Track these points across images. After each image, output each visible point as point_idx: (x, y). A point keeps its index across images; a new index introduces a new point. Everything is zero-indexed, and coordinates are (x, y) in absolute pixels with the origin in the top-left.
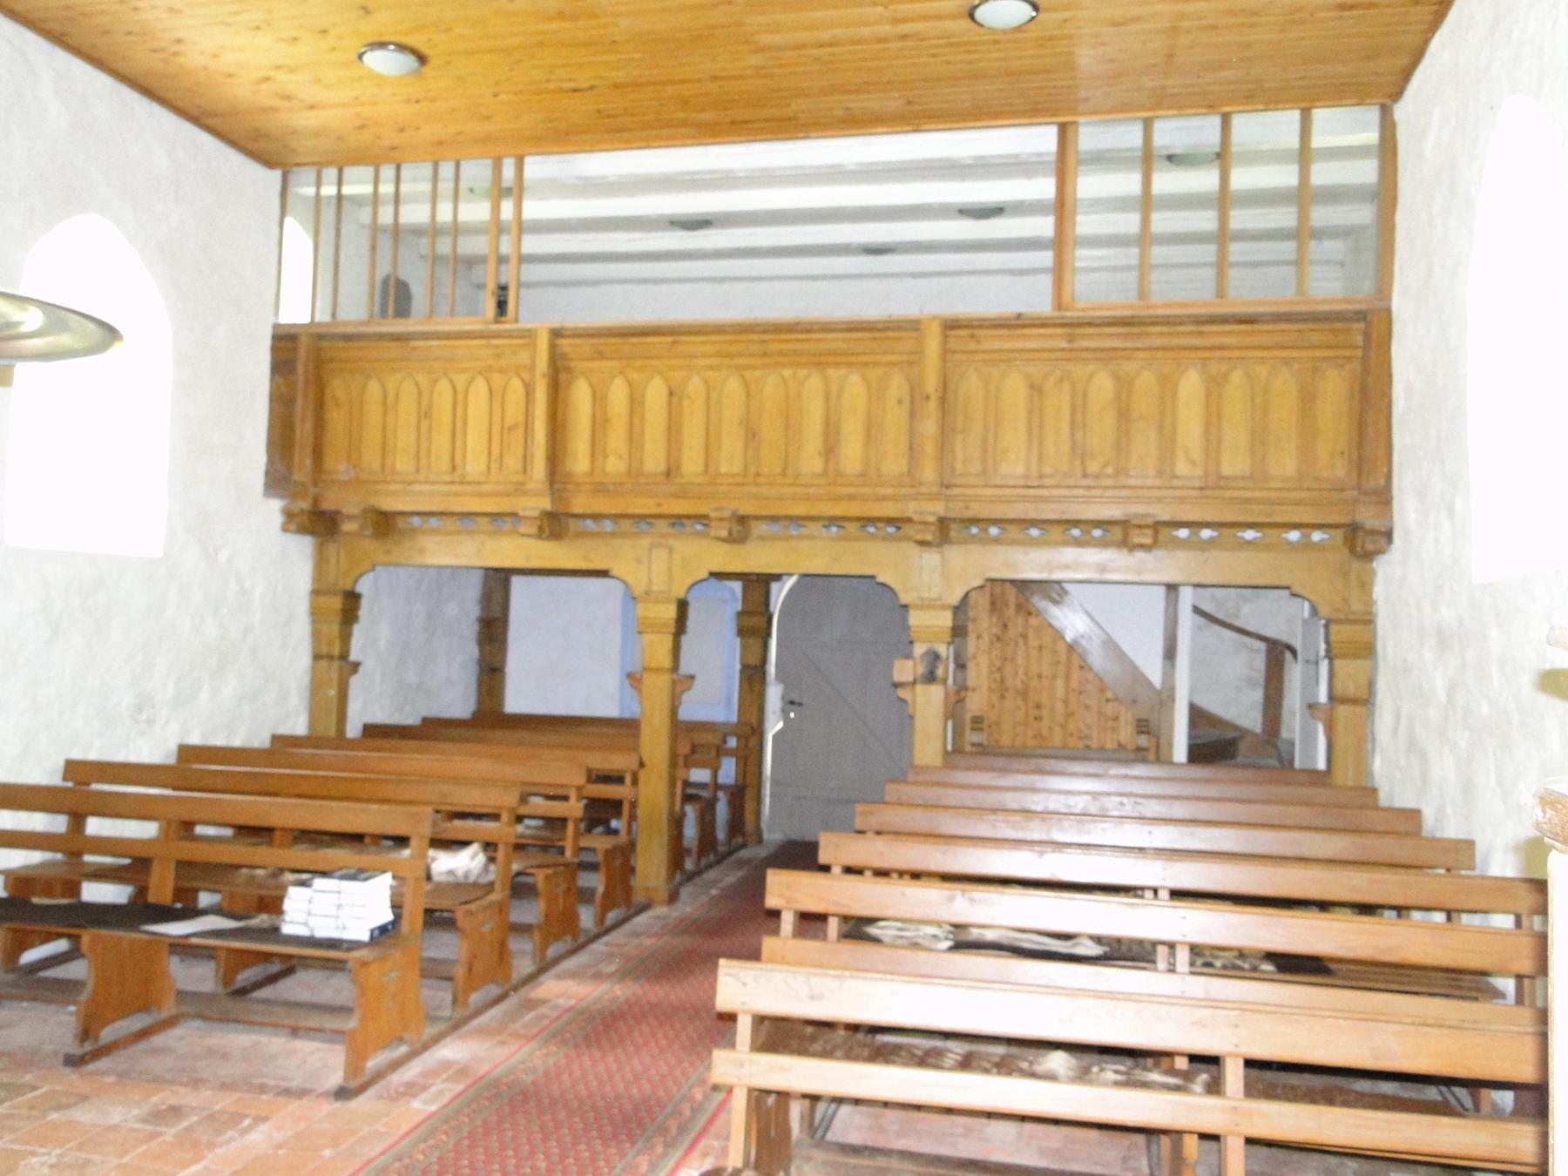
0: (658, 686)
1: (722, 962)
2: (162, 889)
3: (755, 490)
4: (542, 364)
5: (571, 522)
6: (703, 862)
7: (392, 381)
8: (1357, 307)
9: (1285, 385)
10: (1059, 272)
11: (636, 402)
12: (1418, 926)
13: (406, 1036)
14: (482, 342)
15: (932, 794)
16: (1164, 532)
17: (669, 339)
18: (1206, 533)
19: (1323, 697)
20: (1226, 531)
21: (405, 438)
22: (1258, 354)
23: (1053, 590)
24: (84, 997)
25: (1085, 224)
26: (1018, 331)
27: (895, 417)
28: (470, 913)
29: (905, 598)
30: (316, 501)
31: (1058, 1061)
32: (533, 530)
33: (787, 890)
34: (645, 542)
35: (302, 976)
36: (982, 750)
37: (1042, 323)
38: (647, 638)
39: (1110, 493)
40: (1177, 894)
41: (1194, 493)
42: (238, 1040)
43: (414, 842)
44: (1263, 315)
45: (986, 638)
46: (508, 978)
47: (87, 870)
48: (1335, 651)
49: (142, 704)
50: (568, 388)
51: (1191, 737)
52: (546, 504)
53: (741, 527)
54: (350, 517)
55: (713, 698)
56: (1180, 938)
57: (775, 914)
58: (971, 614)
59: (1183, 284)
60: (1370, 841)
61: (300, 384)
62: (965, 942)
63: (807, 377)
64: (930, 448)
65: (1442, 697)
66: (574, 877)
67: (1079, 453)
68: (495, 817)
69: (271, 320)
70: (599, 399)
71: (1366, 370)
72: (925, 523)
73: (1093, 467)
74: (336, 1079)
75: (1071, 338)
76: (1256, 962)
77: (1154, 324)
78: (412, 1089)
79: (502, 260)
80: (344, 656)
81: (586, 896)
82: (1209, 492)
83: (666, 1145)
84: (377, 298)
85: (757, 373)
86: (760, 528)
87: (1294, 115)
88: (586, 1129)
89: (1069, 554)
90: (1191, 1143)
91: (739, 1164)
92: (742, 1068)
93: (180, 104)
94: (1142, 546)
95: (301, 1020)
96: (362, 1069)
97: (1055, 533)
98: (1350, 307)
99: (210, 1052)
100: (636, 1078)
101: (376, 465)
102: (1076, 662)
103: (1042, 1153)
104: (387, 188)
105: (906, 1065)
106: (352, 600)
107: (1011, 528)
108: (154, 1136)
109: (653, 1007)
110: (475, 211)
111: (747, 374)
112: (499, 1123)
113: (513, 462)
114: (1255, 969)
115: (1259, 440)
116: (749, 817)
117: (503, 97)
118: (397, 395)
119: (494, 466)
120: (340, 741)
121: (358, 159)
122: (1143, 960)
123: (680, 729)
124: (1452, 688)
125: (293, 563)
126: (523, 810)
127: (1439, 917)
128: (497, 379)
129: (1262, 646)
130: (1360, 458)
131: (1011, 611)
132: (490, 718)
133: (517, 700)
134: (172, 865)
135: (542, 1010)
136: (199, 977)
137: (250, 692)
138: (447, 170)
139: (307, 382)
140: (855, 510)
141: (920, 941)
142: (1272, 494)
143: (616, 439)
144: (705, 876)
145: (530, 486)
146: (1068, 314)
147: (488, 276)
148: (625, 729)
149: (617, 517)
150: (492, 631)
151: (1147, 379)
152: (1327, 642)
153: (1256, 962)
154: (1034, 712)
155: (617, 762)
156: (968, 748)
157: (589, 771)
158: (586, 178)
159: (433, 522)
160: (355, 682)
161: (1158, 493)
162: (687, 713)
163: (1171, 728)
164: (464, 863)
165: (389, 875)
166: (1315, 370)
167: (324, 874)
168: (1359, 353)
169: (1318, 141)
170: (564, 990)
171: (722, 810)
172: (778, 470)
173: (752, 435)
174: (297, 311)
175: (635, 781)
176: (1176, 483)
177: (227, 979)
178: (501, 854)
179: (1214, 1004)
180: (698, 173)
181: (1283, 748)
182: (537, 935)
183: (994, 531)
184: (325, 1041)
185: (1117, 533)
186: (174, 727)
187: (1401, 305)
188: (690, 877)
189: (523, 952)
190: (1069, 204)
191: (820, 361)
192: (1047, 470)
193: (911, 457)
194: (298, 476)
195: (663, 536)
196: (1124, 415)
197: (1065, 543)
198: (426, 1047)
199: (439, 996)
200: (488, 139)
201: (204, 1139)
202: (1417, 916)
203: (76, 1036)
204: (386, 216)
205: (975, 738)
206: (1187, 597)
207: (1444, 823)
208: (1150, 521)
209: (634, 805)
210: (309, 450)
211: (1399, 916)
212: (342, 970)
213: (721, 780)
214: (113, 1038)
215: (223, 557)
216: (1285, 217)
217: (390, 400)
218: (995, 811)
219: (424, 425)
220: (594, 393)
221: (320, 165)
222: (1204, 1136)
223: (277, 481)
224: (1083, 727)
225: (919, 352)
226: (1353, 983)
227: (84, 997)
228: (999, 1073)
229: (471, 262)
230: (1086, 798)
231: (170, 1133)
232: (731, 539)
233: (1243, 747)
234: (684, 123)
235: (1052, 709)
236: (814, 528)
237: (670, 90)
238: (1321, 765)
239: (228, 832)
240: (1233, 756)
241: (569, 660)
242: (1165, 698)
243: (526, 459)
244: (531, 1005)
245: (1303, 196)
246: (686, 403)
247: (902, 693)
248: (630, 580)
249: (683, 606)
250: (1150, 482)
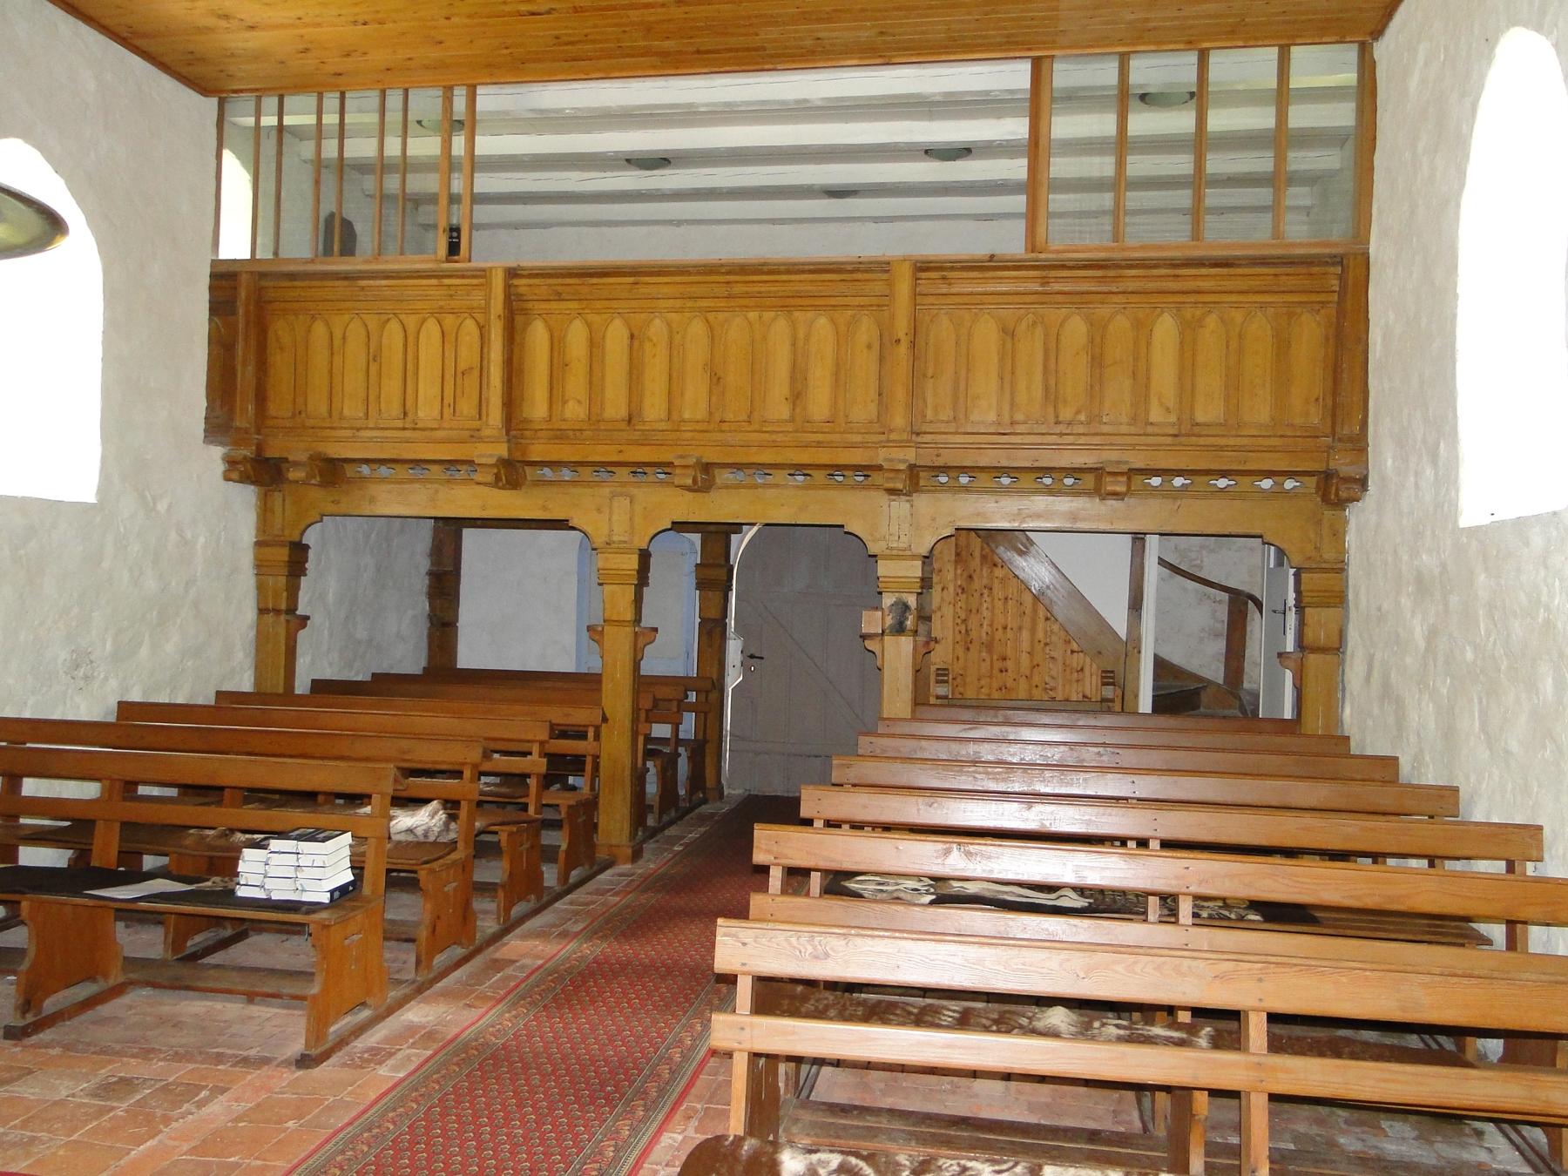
0: (619, 641)
1: (720, 921)
2: (105, 851)
3: (719, 436)
4: (497, 306)
5: (528, 470)
6: (665, 818)
7: (338, 322)
8: (1334, 251)
9: (1260, 328)
10: (1032, 216)
11: (595, 345)
12: (1395, 871)
13: (369, 1001)
14: (434, 282)
15: (906, 746)
16: (1137, 480)
17: (631, 280)
18: (1178, 482)
19: (1290, 646)
20: (1198, 479)
21: (353, 381)
22: (1234, 298)
23: (1018, 539)
24: (25, 966)
25: (1061, 167)
26: (991, 274)
27: (864, 364)
28: (432, 871)
29: (873, 549)
30: (260, 448)
31: (1058, 1017)
32: (490, 478)
33: (773, 845)
34: (606, 491)
35: (254, 939)
36: (947, 702)
37: (1017, 265)
38: (607, 588)
39: (1083, 440)
40: (1167, 845)
41: (1169, 440)
42: (193, 1007)
43: (376, 798)
44: (1238, 258)
45: (951, 589)
46: (472, 939)
47: (22, 833)
48: (1306, 600)
49: (80, 660)
50: (524, 330)
51: (1155, 689)
52: (502, 450)
53: (705, 476)
54: (296, 464)
55: (672, 654)
56: (1184, 890)
57: (764, 870)
59: (1159, 229)
60: (1356, 788)
61: (241, 326)
62: (946, 894)
63: (774, 319)
64: (900, 394)
65: (1422, 644)
66: (537, 835)
67: (1052, 396)
68: (458, 774)
69: (211, 257)
70: (557, 343)
71: (1341, 313)
72: (899, 471)
73: (1066, 413)
74: (297, 1047)
75: (1045, 281)
76: (1243, 912)
77: (1130, 267)
78: (377, 1055)
79: (454, 199)
80: (292, 610)
81: (550, 854)
82: (1183, 439)
83: (646, 1109)
84: (321, 238)
85: (721, 316)
86: (723, 476)
87: (1272, 53)
88: (562, 1095)
89: (1040, 502)
90: (1201, 1101)
91: (741, 1133)
92: (742, 1031)
93: (107, 22)
94: (1116, 495)
95: (260, 986)
96: (326, 1035)
97: (1027, 481)
98: (1327, 251)
99: (162, 1021)
100: (611, 1040)
101: (324, 409)
102: (1042, 613)
103: (1032, 1108)
104: (330, 119)
105: (902, 1024)
106: (299, 552)
107: (982, 476)
108: (102, 1111)
109: (623, 967)
110: (425, 146)
111: (711, 316)
112: (471, 1090)
113: (467, 407)
114: (1241, 919)
115: (1234, 384)
116: (709, 773)
117: (455, 20)
118: (344, 338)
119: (448, 412)
120: (288, 695)
121: (300, 87)
122: (1131, 913)
123: (642, 683)
124: (1432, 634)
125: (238, 512)
126: (486, 767)
127: (1424, 863)
128: (449, 320)
129: (1225, 596)
130: (1335, 406)
131: (976, 562)
132: (443, 673)
133: (469, 655)
134: (117, 827)
135: (509, 971)
136: (147, 943)
137: (196, 650)
138: (394, 100)
139: (247, 323)
140: (824, 457)
141: (902, 895)
142: (1245, 441)
143: (576, 384)
144: (667, 832)
145: (487, 432)
146: (1043, 256)
147: (441, 216)
148: (585, 684)
149: (576, 465)
150: (444, 585)
151: (1121, 324)
152: (1298, 591)
153: (1243, 912)
154: (998, 665)
155: (579, 716)
156: (933, 700)
157: (552, 726)
158: (542, 111)
159: (384, 471)
160: (302, 635)
161: (1129, 440)
162: (647, 669)
163: (1137, 678)
164: (421, 821)
165: (347, 838)
166: (1291, 315)
167: (282, 835)
168: (1336, 297)
169: (1296, 82)
170: (531, 949)
171: (683, 766)
172: (744, 417)
173: (716, 379)
174: (236, 244)
175: (597, 737)
176: (1150, 429)
177: (177, 944)
178: (463, 812)
179: (1239, 956)
180: (657, 106)
181: (1246, 698)
182: (501, 894)
183: (964, 480)
184: (287, 1007)
185: (1089, 481)
186: (113, 683)
187: (1378, 248)
188: (653, 833)
189: (486, 912)
190: (1043, 142)
191: (786, 304)
192: (1019, 417)
193: (880, 403)
194: (240, 422)
195: (623, 484)
196: (1097, 361)
197: (1036, 492)
198: (390, 1011)
199: (403, 959)
200: (440, 66)
201: (159, 1112)
202: (1391, 862)
203: (16, 1008)
204: (330, 149)
205: (941, 690)
206: (1152, 542)
207: (1423, 768)
208: (1125, 468)
209: (596, 758)
210: (251, 395)
211: (1375, 862)
212: (299, 933)
213: (682, 736)
214: (59, 1007)
215: (162, 507)
216: (1260, 162)
217: (337, 342)
218: (975, 763)
219: (373, 368)
220: (552, 337)
221: (259, 93)
222: (1215, 1093)
223: (217, 428)
224: (1047, 679)
225: (890, 296)
226: (1410, 937)
227: (25, 966)
228: (999, 1031)
229: (416, 201)
230: (1062, 748)
231: (121, 1107)
232: (693, 489)
233: (1204, 697)
234: (647, 52)
235: (1018, 662)
236: (780, 476)
237: (634, 15)
238: (1288, 714)
239: (173, 792)
240: (1195, 707)
241: (527, 611)
242: (1133, 645)
243: (481, 402)
244: (498, 965)
245: (1280, 139)
246: (647, 346)
247: (869, 644)
248: (588, 529)
249: (645, 556)
250: (1124, 429)
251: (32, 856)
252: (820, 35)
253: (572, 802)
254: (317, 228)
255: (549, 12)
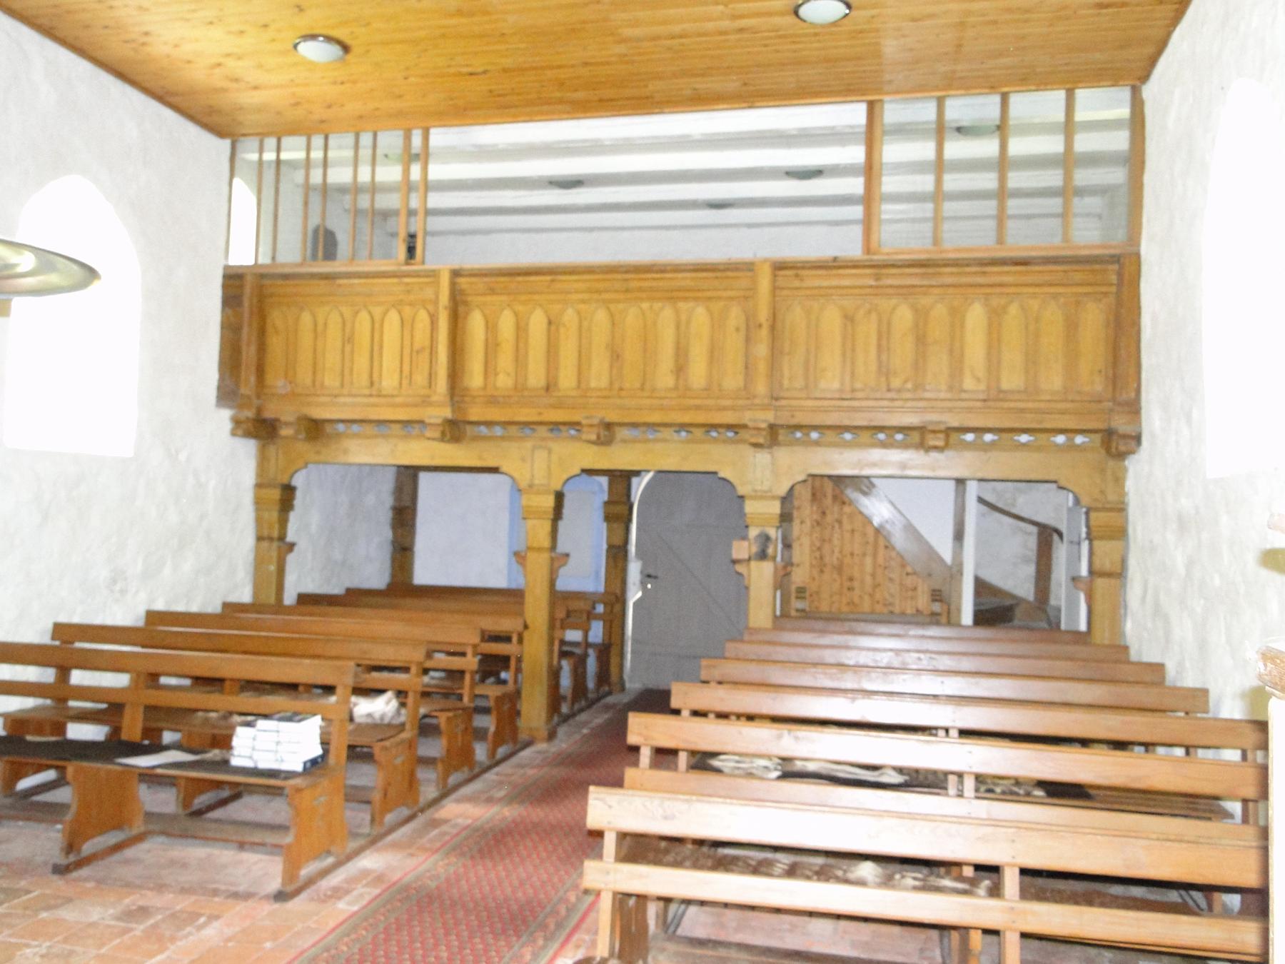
0: (539, 562)
1: (592, 788)
2: (132, 729)
3: (618, 401)
4: (444, 298)
5: (468, 428)
6: (576, 707)
7: (321, 312)
8: (1112, 252)
9: (1053, 315)
10: (868, 223)
11: (521, 329)
12: (1162, 759)
13: (333, 849)
14: (395, 280)
15: (764, 651)
16: (954, 436)
17: (549, 278)
18: (988, 437)
19: (1084, 571)
20: (1005, 436)
21: (332, 359)
22: (1031, 290)
23: (863, 484)
24: (69, 817)
25: (889, 184)
26: (834, 272)
27: (733, 342)
28: (385, 748)
29: (741, 490)
30: (259, 410)
31: (867, 870)
32: (437, 434)
33: (645, 730)
34: (529, 444)
35: (247, 800)
36: (805, 615)
37: (854, 265)
38: (530, 523)
39: (909, 404)
40: (965, 733)
41: (979, 404)
42: (195, 852)
43: (339, 690)
44: (1035, 258)
45: (808, 523)
46: (416, 801)
47: (71, 713)
48: (1094, 534)
49: (117, 577)
50: (465, 318)
51: (976, 604)
52: (447, 413)
53: (607, 432)
54: (287, 424)
55: (584, 572)
56: (967, 769)
57: (635, 749)
58: (796, 503)
59: (970, 233)
60: (1122, 689)
61: (246, 315)
62: (791, 772)
63: (662, 309)
64: (762, 367)
65: (1182, 571)
66: (470, 719)
67: (885, 371)
68: (406, 670)
69: (222, 263)
70: (491, 327)
71: (1119, 303)
72: (758, 429)
73: (896, 383)
74: (275, 884)
75: (878, 277)
76: (1030, 789)
77: (946, 265)
78: (338, 893)
79: (411, 213)
80: (282, 538)
81: (480, 734)
82: (991, 404)
83: (546, 939)
84: (309, 244)
85: (621, 306)
86: (623, 433)
87: (1061, 95)
88: (480, 926)
89: (876, 454)
90: (976, 937)
91: (606, 954)
92: (608, 875)
93: (147, 85)
94: (936, 448)
95: (247, 837)
96: (297, 876)
97: (865, 437)
98: (1107, 252)
99: (172, 863)
100: (521, 884)
101: (308, 381)
102: (882, 542)
103: (854, 945)
104: (317, 154)
105: (742, 873)
106: (288, 492)
107: (829, 433)
108: (126, 931)
109: (535, 825)
110: (390, 173)
111: (612, 306)
112: (409, 920)
113: (420, 379)
114: (1028, 794)
115: (1032, 360)
116: (614, 670)
117: (412, 79)
118: (325, 324)
119: (405, 382)
120: (279, 607)
121: (293, 130)
123: (557, 598)
124: (1190, 564)
125: (240, 462)
126: (428, 664)
127: (1179, 752)
128: (408, 311)
129: (1034, 529)
130: (1115, 376)
131: (829, 501)
132: (402, 589)
133: (424, 574)
134: (141, 709)
135: (444, 828)
136: (163, 801)
137: (205, 567)
138: (366, 139)
139: (251, 313)
140: (701, 418)
141: (754, 771)
142: (1042, 405)
143: (505, 360)
144: (577, 718)
145: (434, 398)
146: (875, 257)
147: (400, 226)
148: (512, 597)
149: (506, 424)
150: (404, 517)
151: (940, 311)
152: (1088, 526)
153: (1030, 789)
154: (847, 584)
155: (506, 624)
156: (793, 613)
157: (483, 632)
158: (480, 146)
159: (355, 428)
160: (291, 559)
161: (949, 404)
162: (563, 584)
163: (960, 597)
164: (380, 707)
165: (318, 718)
166: (1078, 303)
167: (266, 716)
168: (1114, 289)
169: (1080, 116)
170: (462, 812)
171: (592, 664)
172: (638, 385)
173: (616, 357)
174: (244, 255)
175: (520, 641)
176: (964, 396)
177: (186, 803)
178: (410, 700)
179: (995, 823)
180: (572, 141)
181: (1051, 613)
182: (440, 767)
183: (814, 435)
184: (267, 853)
185: (916, 437)
186: (143, 596)
187: (1148, 250)
188: (566, 719)
189: (429, 780)
190: (876, 167)
191: (672, 296)
192: (858, 385)
193: (747, 375)
194: (244, 390)
195: (543, 439)
196: (921, 340)
197: (873, 445)
198: (349, 858)
199: (360, 817)
200: (400, 114)
201: (168, 933)
202: (1161, 750)
203: (62, 849)
204: (316, 177)
205: (799, 605)
206: (972, 489)
207: (1184, 674)
208: (942, 427)
209: (519, 660)
210: (253, 369)
211: (1147, 751)
212: (281, 795)
213: (591, 639)
214: (93, 851)
215: (182, 457)
216: (1053, 178)
217: (320, 328)
218: (815, 665)
219: (348, 348)
220: (487, 323)
221: (262, 136)
222: (987, 932)
223: (227, 394)
224: (887, 596)
225: (753, 289)
226: (1109, 806)
227: (69, 817)
228: (819, 880)
229: (386, 215)
230: (890, 654)
231: (139, 929)
232: (599, 442)
233: (1018, 612)
234: (561, 101)
235: (862, 582)
236: (667, 433)
237: (549, 73)
238: (1083, 627)
239: (187, 682)
240: (1010, 620)
241: (467, 541)
242: (955, 572)
243: (431, 376)
244: (435, 823)
245: (1068, 161)
246: (562, 330)
247: (739, 568)
248: (516, 475)
249: (559, 497)
250: (942, 395)
251: (78, 732)
252: (697, 86)
253: (499, 694)
254: (305, 242)
255: (485, 72)
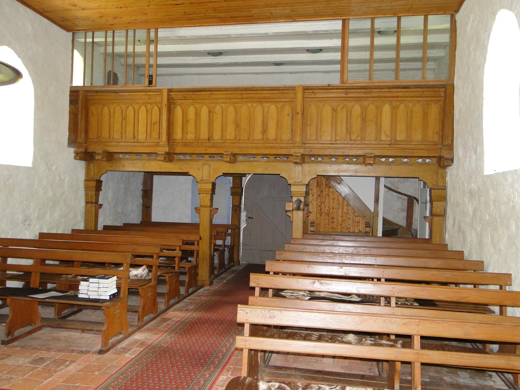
0: (205, 212)
1: (239, 305)
2: (35, 282)
3: (238, 145)
4: (165, 101)
5: (175, 156)
6: (221, 271)
7: (112, 107)
8: (442, 83)
9: (418, 109)
10: (342, 72)
11: (197, 114)
12: (463, 289)
13: (122, 332)
14: (144, 93)
15: (301, 247)
16: (377, 159)
17: (209, 93)
18: (391, 160)
19: (428, 214)
20: (397, 159)
21: (117, 126)
22: (409, 99)
23: (338, 179)
24: (8, 320)
25: (352, 55)
26: (329, 91)
27: (287, 121)
28: (143, 289)
29: (290, 182)
30: (86, 149)
31: (351, 337)
32: (162, 159)
33: (256, 280)
34: (201, 163)
35: (84, 311)
36: (314, 233)
37: (337, 88)
38: (201, 195)
39: (359, 146)
40: (387, 280)
41: (388, 146)
42: (64, 334)
43: (125, 265)
44: (411, 86)
45: (315, 195)
46: (156, 311)
47: (7, 276)
48: (433, 199)
49: (26, 219)
50: (174, 109)
51: (383, 228)
52: (167, 149)
53: (234, 158)
54: (98, 154)
55: (223, 217)
56: (393, 295)
57: (253, 288)
58: (310, 188)
59: (384, 76)
60: (450, 261)
61: (80, 108)
62: (314, 296)
63: (257, 106)
64: (299, 131)
65: (472, 214)
66: (178, 277)
67: (349, 131)
68: (152, 257)
69: (70, 85)
70: (185, 114)
71: (445, 104)
72: (298, 156)
73: (354, 137)
74: (99, 347)
75: (347, 93)
76: (412, 303)
77: (375, 89)
78: (125, 350)
79: (150, 66)
80: (97, 202)
81: (182, 283)
82: (392, 146)
83: (214, 368)
84: (106, 79)
85: (239, 105)
86: (240, 158)
87: (422, 18)
88: (186, 363)
89: (345, 167)
90: (398, 365)
91: (246, 376)
92: (246, 342)
93: (35, 7)
94: (370, 164)
95: (86, 327)
96: (108, 343)
97: (340, 159)
98: (440, 83)
99: (54, 339)
100: (203, 345)
101: (107, 136)
102: (345, 203)
103: (342, 367)
104: (110, 39)
105: (299, 340)
106: (99, 183)
107: (326, 158)
108: (34, 369)
109: (207, 321)
110: (141, 48)
111: (236, 105)
112: (156, 361)
113: (155, 135)
114: (412, 305)
115: (409, 127)
116: (235, 256)
117: (151, 7)
118: (114, 112)
119: (148, 137)
120: (96, 231)
121: (100, 29)
123: (213, 227)
124: (475, 210)
125: (79, 170)
126: (161, 254)
127: (472, 286)
128: (149, 106)
129: (406, 198)
130: (443, 135)
131: (324, 186)
132: (147, 223)
133: (156, 217)
134: (39, 274)
135: (169, 322)
136: (49, 313)
137: (65, 215)
138: (131, 33)
139: (82, 107)
140: (273, 152)
141: (299, 297)
142: (413, 146)
143: (191, 127)
144: (221, 276)
145: (161, 143)
146: (346, 85)
147: (146, 72)
148: (194, 227)
149: (191, 154)
150: (147, 194)
151: (372, 108)
152: (430, 196)
153: (412, 303)
154: (331, 220)
155: (192, 237)
156: (309, 232)
157: (183, 241)
158: (180, 37)
159: (127, 156)
160: (100, 211)
161: (374, 146)
162: (215, 222)
163: (377, 225)
164: (140, 272)
165: (115, 278)
166: (428, 104)
167: (93, 277)
168: (443, 99)
169: (430, 27)
170: (176, 315)
171: (227, 254)
172: (247, 138)
173: (237, 126)
174: (78, 81)
175: (198, 244)
176: (381, 142)
177: (59, 313)
178: (154, 269)
179: (411, 317)
180: (218, 35)
181: (413, 232)
182: (166, 296)
183: (320, 159)
184: (95, 334)
185: (361, 160)
186: (38, 227)
187: (457, 82)
188: (217, 276)
189: (161, 303)
190: (346, 47)
191: (261, 101)
192: (338, 138)
193: (292, 134)
194: (80, 140)
195: (207, 161)
196: (364, 120)
197: (344, 163)
198: (129, 335)
199: (134, 318)
200: (146, 22)
201: (53, 369)
202: (461, 286)
203: (5, 334)
204: (109, 49)
205: (312, 229)
206: (382, 180)
207: (472, 255)
208: (373, 155)
209: (198, 251)
210: (83, 131)
211: (456, 286)
212: (99, 309)
213: (226, 244)
214: (20, 334)
215: (54, 168)
216: (418, 54)
217: (112, 114)
218: (323, 253)
219: (124, 122)
220: (183, 112)
221: (86, 31)
222: (403, 362)
223: (72, 142)
224: (347, 225)
225: (295, 98)
226: (468, 311)
227: (8, 320)
228: (331, 342)
229: (138, 67)
230: (352, 248)
231: (40, 367)
232: (230, 162)
233: (399, 231)
234: (214, 17)
235: (338, 220)
236: (259, 158)
237: (210, 5)
238: (427, 237)
239: (57, 263)
240: (396, 234)
241: (175, 203)
242: (376, 214)
243: (159, 133)
244: (165, 320)
245: (425, 46)
246: (215, 115)
247: (288, 214)
248: (195, 176)
249: (214, 185)
250: (373, 142)
255: (182, 4)
